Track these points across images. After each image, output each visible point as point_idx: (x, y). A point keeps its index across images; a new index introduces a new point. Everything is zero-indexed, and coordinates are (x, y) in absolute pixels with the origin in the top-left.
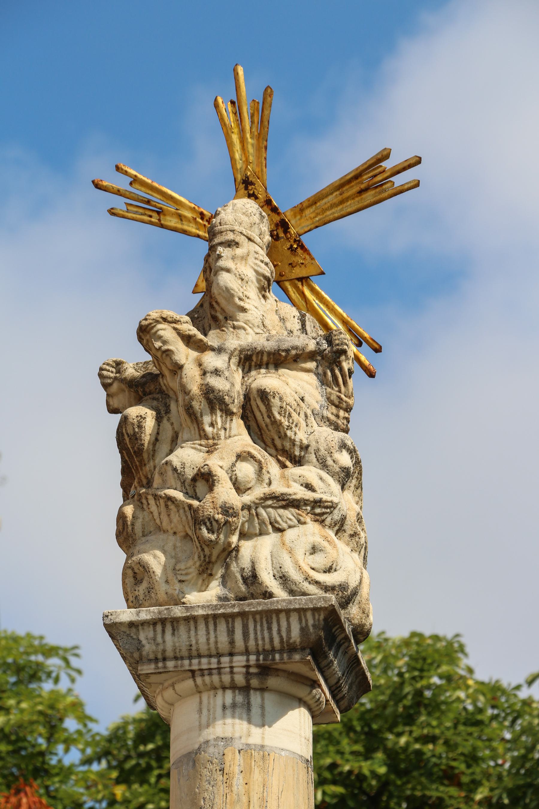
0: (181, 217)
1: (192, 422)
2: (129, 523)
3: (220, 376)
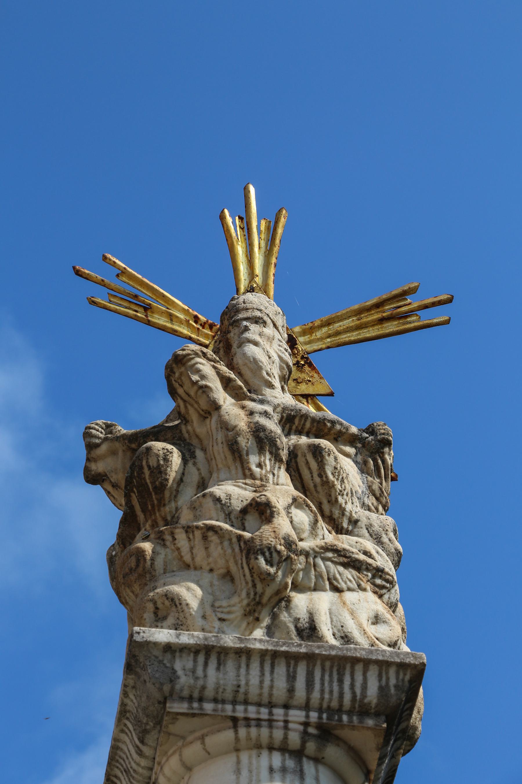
0: (171, 317)
1: (234, 459)
2: (148, 558)
3: (270, 419)
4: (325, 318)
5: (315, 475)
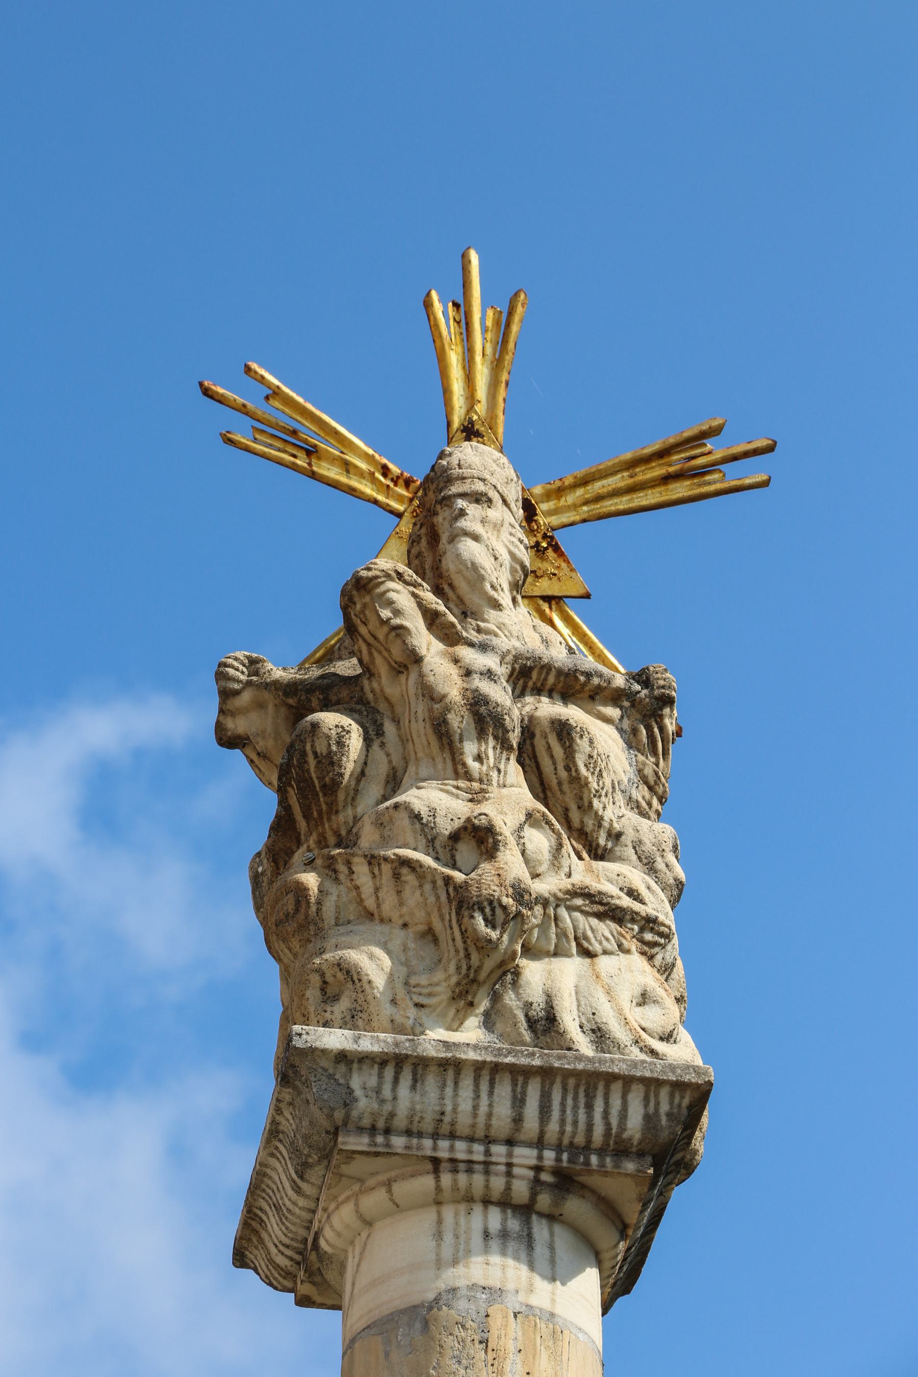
0: (347, 467)
1: (442, 747)
2: (313, 900)
3: (495, 682)
4: (580, 472)
5: (560, 767)
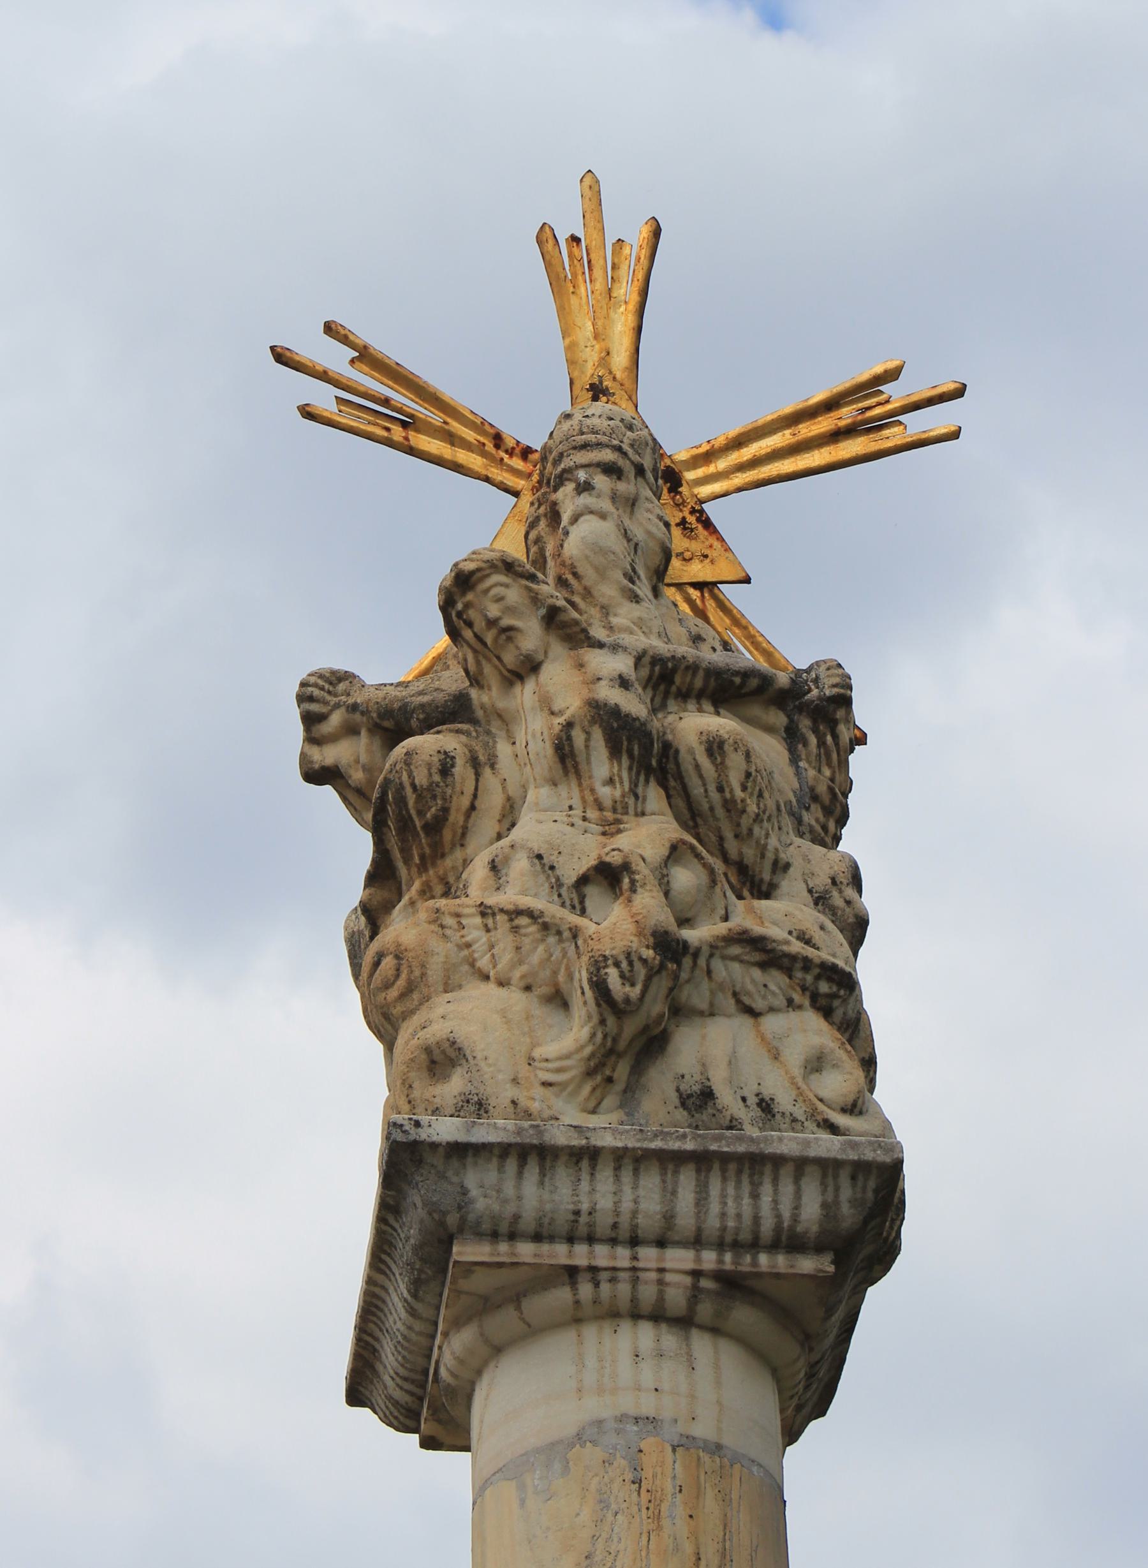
4: (733, 432)
